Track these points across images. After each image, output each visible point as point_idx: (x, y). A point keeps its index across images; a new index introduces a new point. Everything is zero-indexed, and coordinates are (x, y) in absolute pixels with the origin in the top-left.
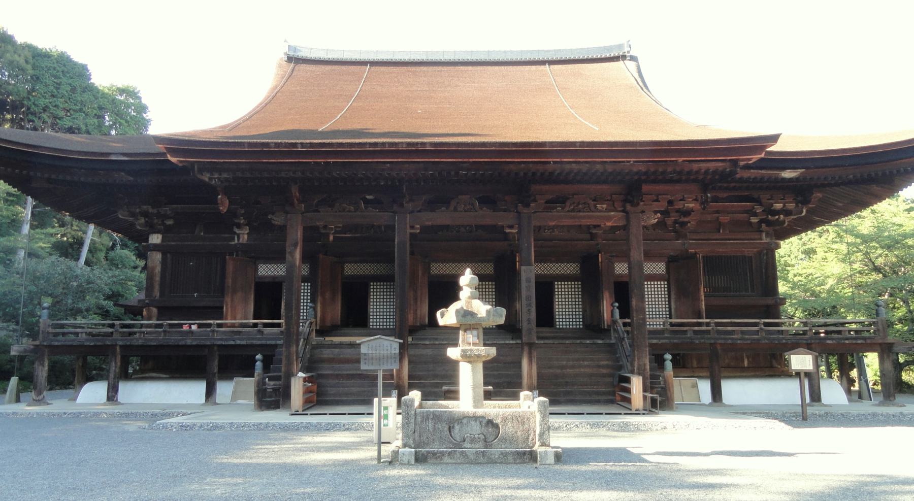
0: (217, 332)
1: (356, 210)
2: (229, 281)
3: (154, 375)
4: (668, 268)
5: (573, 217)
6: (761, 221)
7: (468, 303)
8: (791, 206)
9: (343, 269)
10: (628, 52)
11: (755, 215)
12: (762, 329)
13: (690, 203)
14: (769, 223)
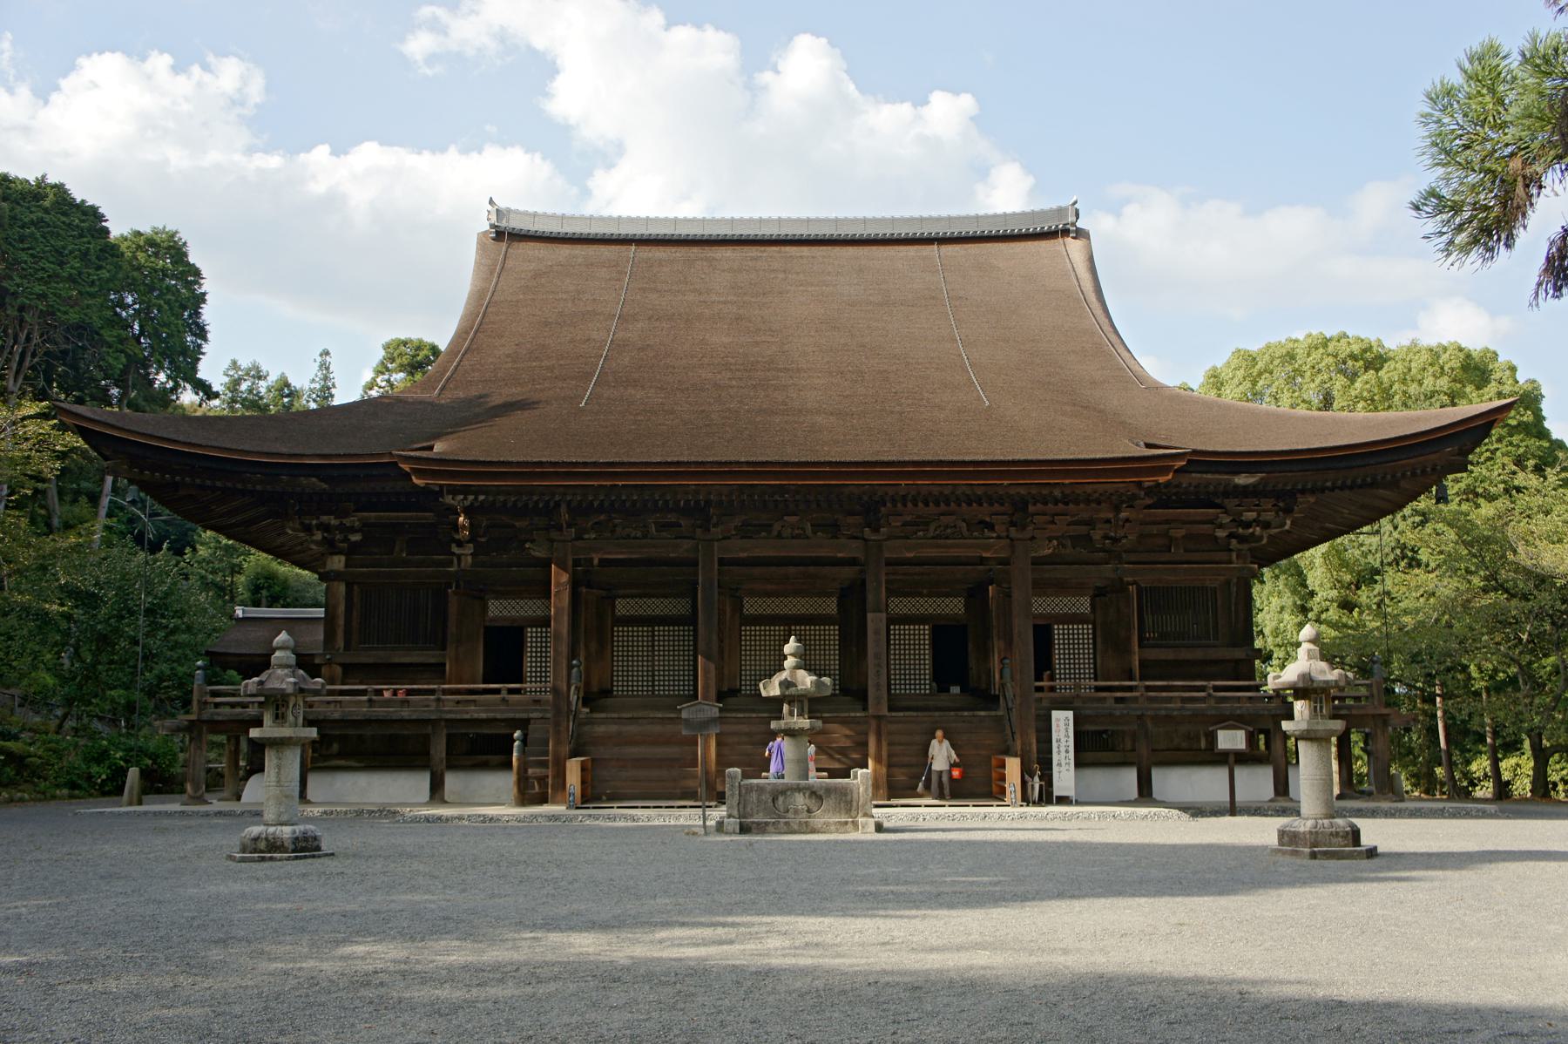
1: (645, 537)
2: (452, 628)
4: (1093, 605)
5: (939, 546)
6: (1231, 536)
7: (793, 674)
8: (1269, 516)
9: (614, 607)
10: (1073, 224)
11: (1221, 526)
14: (1242, 539)
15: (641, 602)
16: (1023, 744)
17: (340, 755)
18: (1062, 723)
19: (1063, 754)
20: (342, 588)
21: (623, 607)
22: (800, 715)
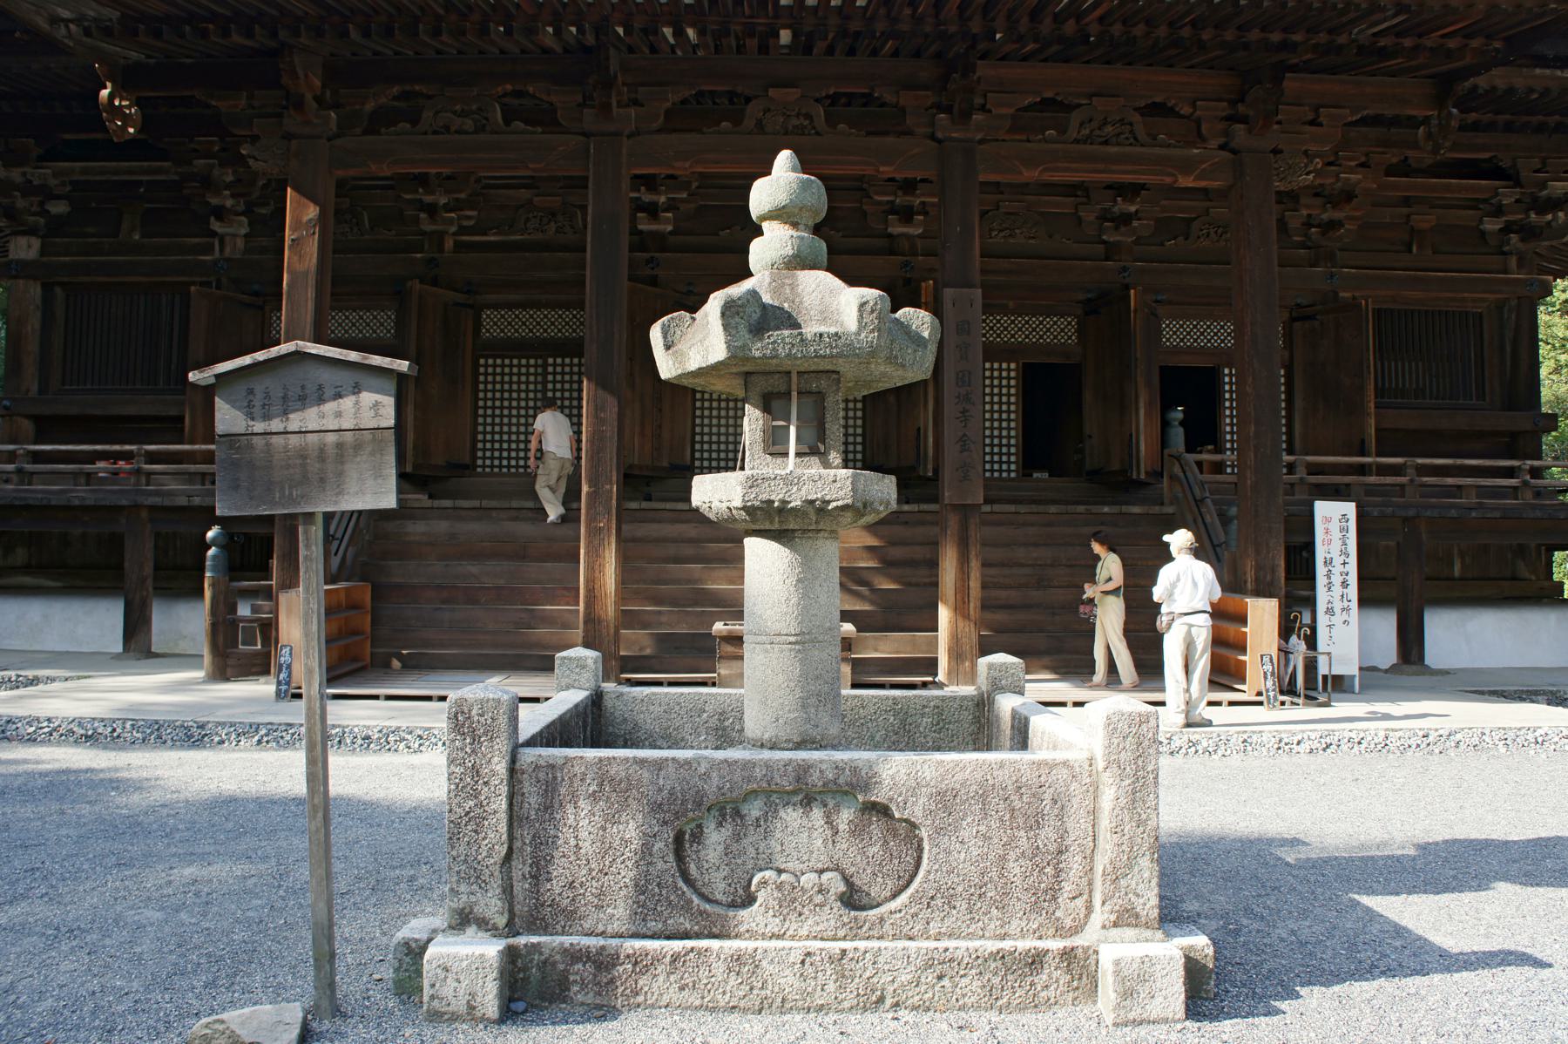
0: (149, 474)
1: (480, 129)
3: (28, 580)
6: (1507, 229)
9: (478, 325)
11: (1498, 211)
12: (1525, 483)
13: (1351, 171)
14: (1530, 233)
15: (524, 315)
16: (1258, 568)
17: (27, 569)
18: (1335, 525)
19: (1337, 590)
20: (35, 290)
21: (495, 324)
22: (813, 449)
